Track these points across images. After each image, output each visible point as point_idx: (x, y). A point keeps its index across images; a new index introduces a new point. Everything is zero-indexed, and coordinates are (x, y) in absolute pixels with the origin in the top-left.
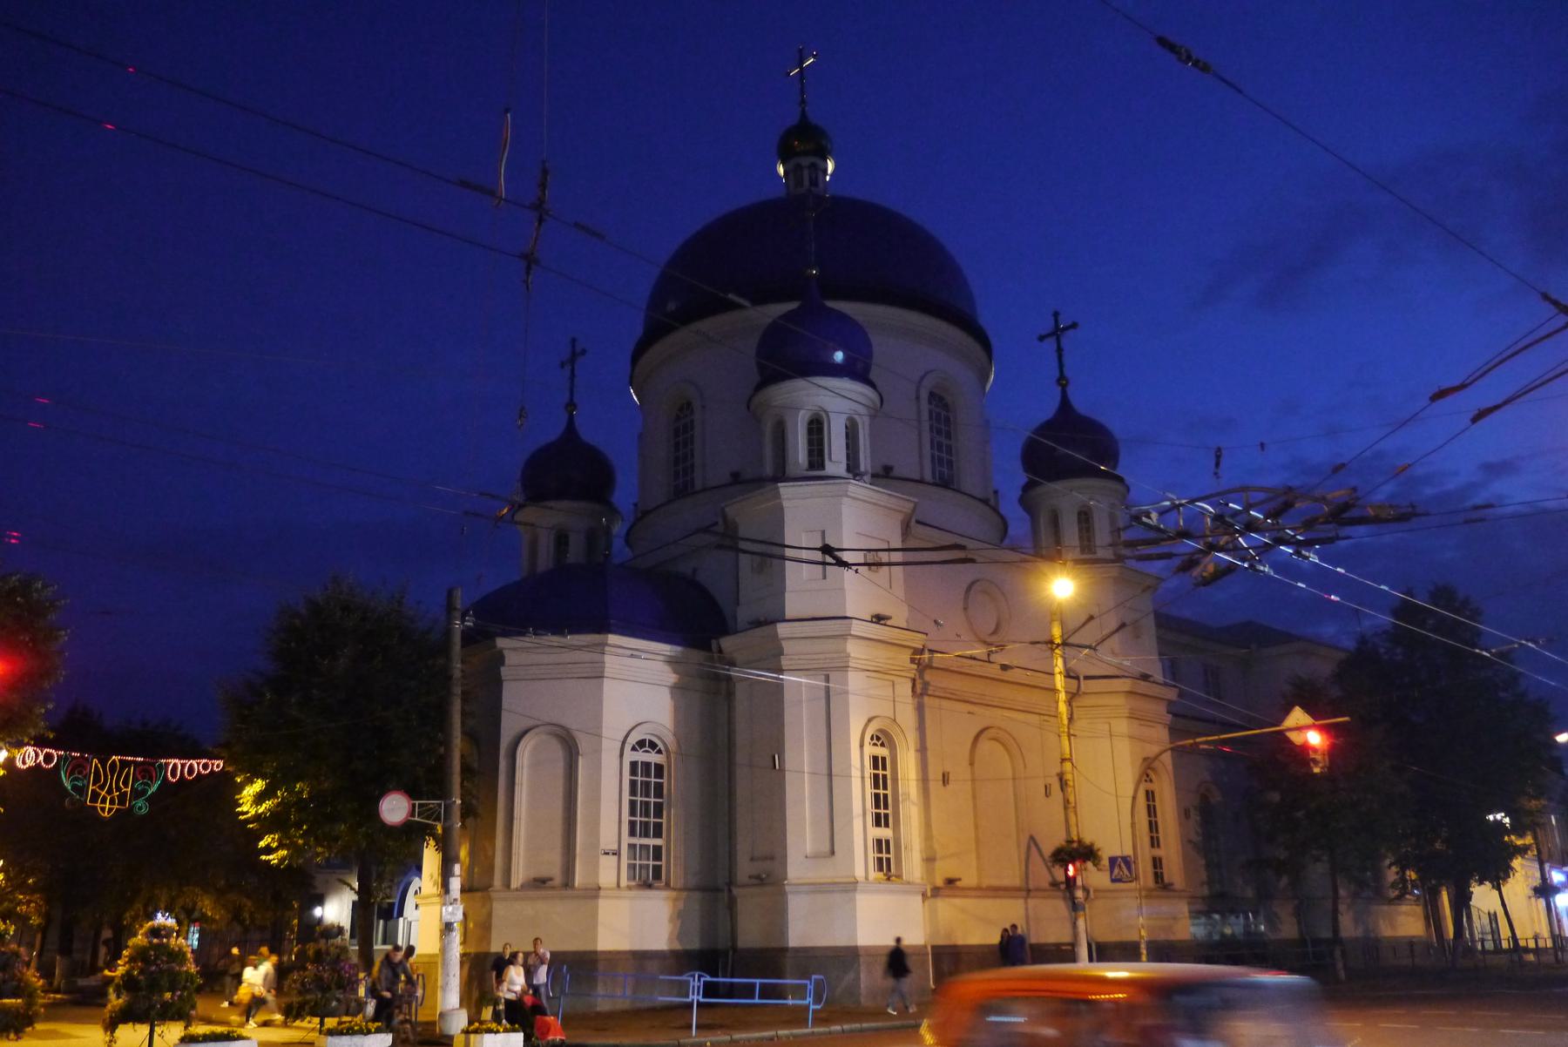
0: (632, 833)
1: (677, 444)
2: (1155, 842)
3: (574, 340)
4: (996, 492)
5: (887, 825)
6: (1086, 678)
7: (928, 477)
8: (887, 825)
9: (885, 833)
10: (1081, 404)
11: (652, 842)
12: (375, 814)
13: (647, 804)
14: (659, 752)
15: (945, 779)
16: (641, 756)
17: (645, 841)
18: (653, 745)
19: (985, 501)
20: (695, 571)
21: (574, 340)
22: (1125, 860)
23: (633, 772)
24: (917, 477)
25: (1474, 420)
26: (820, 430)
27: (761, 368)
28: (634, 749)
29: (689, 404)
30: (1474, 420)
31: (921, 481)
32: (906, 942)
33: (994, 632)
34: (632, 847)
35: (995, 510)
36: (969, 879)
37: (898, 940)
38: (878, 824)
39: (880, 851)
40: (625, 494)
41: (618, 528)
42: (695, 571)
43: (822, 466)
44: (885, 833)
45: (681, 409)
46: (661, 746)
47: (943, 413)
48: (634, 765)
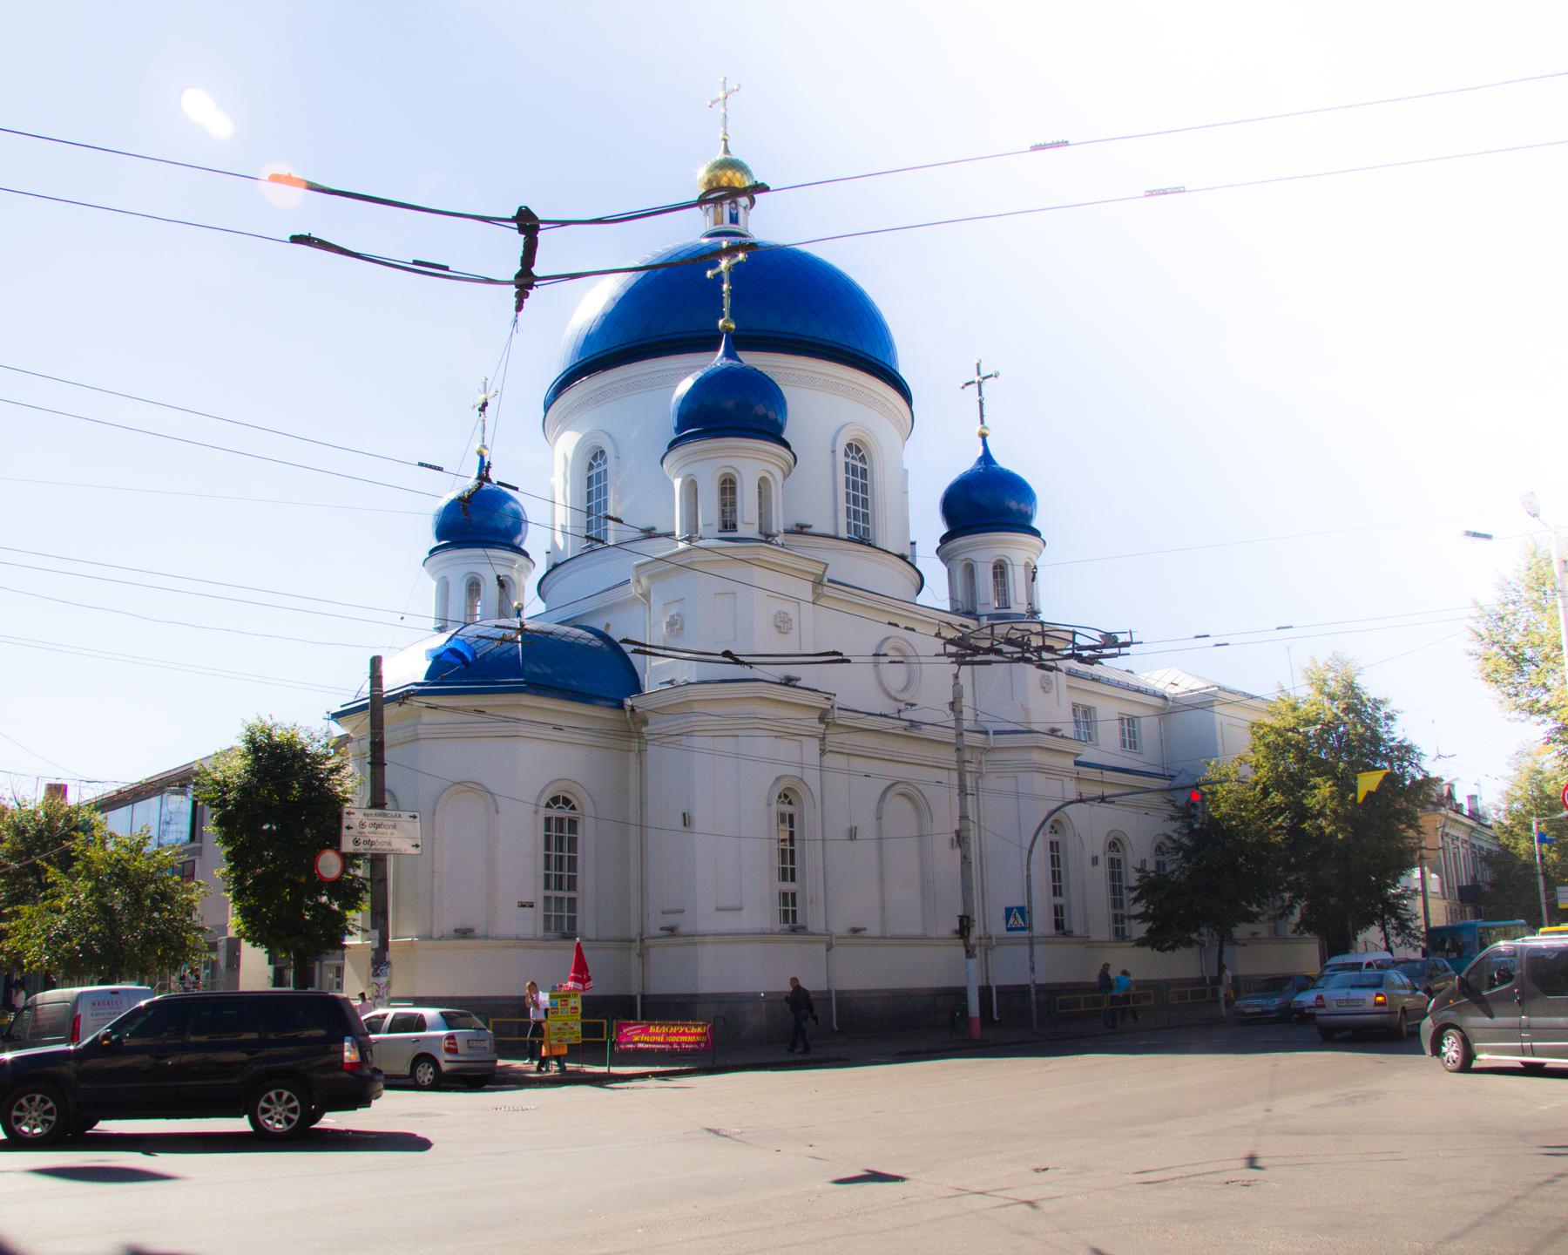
0: (547, 886)
1: (589, 494)
2: (1057, 891)
3: (376, 663)
4: (913, 544)
5: (793, 880)
6: (996, 733)
7: (843, 533)
8: (793, 880)
9: (788, 886)
10: (1003, 461)
11: (565, 894)
12: (313, 865)
13: (561, 838)
14: (573, 808)
15: (852, 834)
16: (555, 813)
17: (559, 894)
18: (567, 802)
19: (903, 557)
20: (608, 626)
21: (376, 663)
22: (1021, 910)
23: (548, 828)
24: (831, 533)
25: (296, 239)
26: (733, 491)
27: (679, 429)
28: (548, 806)
29: (602, 452)
30: (296, 239)
31: (835, 538)
32: (808, 984)
33: (905, 689)
34: (547, 899)
35: (913, 566)
36: (873, 929)
37: (794, 980)
38: (784, 879)
39: (786, 904)
40: (536, 541)
41: (530, 583)
42: (608, 626)
43: (734, 527)
44: (788, 886)
45: (595, 458)
46: (575, 802)
47: (860, 465)
48: (548, 820)
